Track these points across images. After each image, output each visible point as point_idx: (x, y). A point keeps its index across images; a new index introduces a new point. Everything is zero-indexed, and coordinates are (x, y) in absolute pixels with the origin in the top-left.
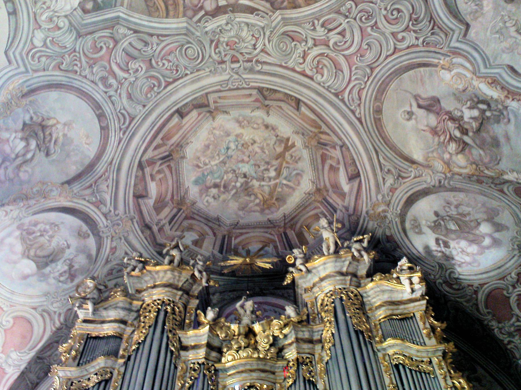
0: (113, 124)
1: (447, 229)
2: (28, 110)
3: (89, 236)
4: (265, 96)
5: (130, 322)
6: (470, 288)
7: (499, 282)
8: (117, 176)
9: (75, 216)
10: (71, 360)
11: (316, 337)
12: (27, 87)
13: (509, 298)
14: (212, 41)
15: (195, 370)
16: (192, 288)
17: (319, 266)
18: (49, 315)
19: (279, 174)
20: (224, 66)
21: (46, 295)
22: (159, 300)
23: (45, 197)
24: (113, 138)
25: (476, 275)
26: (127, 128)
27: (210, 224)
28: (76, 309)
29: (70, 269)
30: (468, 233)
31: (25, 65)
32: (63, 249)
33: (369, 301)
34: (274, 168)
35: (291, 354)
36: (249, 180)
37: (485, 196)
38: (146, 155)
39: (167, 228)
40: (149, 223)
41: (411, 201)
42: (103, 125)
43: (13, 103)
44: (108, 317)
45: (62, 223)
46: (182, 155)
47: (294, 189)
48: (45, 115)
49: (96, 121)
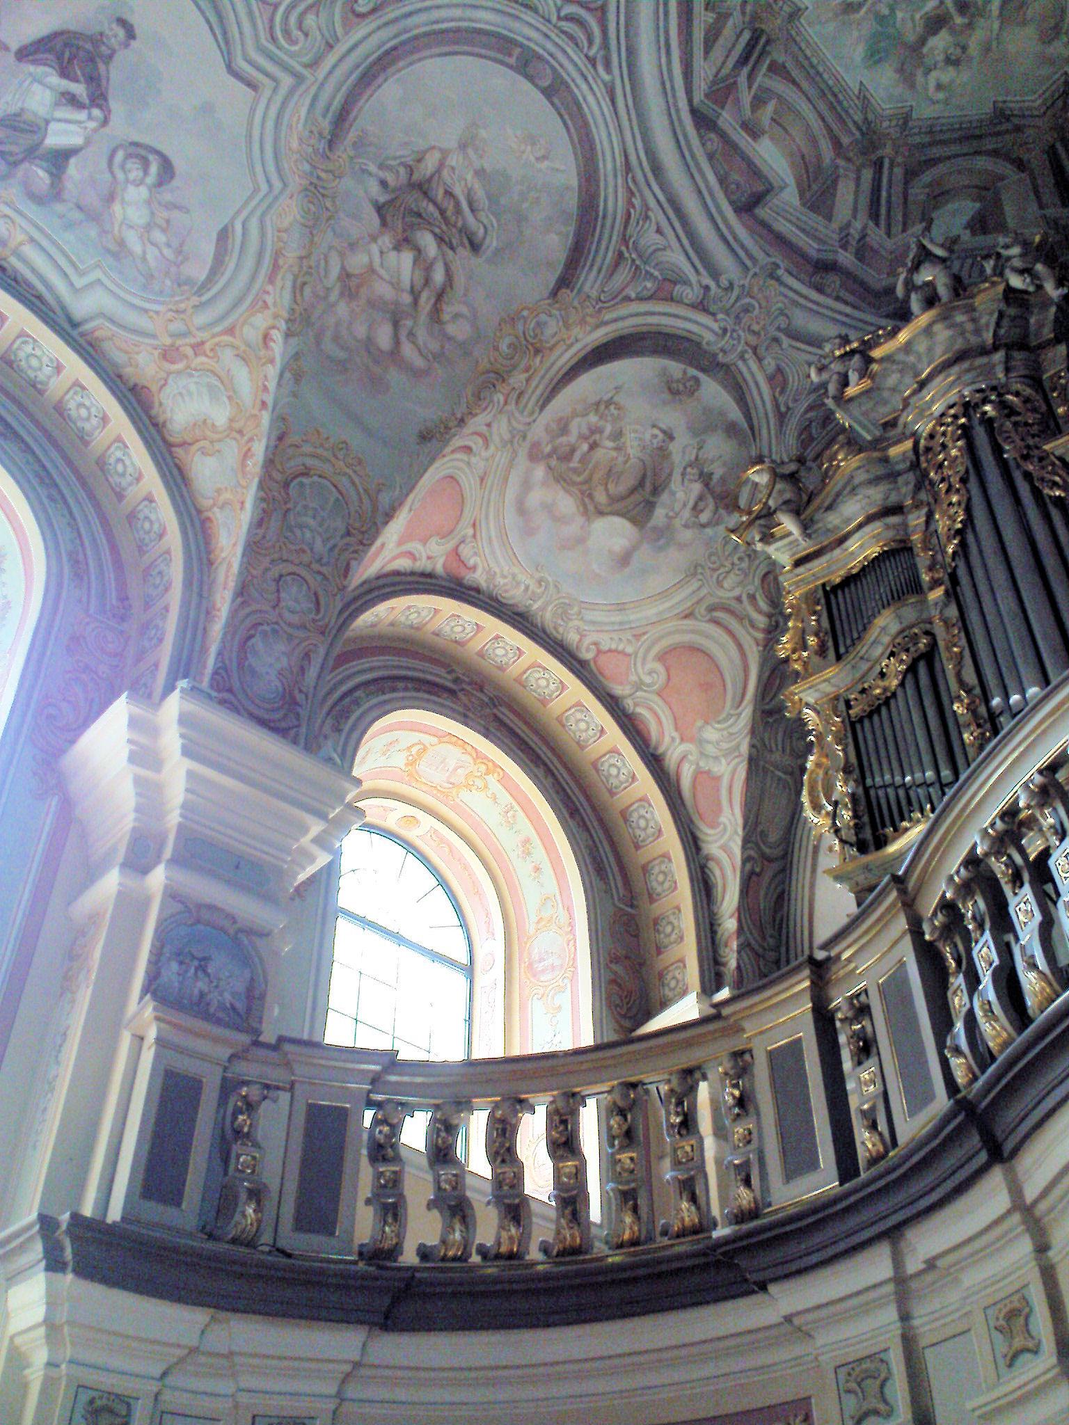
2: (363, 171)
3: (697, 380)
9: (638, 353)
10: (816, 659)
12: (324, 116)
18: (732, 612)
21: (694, 574)
22: (951, 407)
23: (537, 351)
24: (590, 98)
26: (605, 45)
27: (989, 144)
28: (759, 546)
29: (707, 485)
31: (286, 68)
32: (660, 448)
38: (696, 80)
39: (876, 236)
40: (823, 256)
43: (323, 175)
44: (848, 521)
49: (526, 85)
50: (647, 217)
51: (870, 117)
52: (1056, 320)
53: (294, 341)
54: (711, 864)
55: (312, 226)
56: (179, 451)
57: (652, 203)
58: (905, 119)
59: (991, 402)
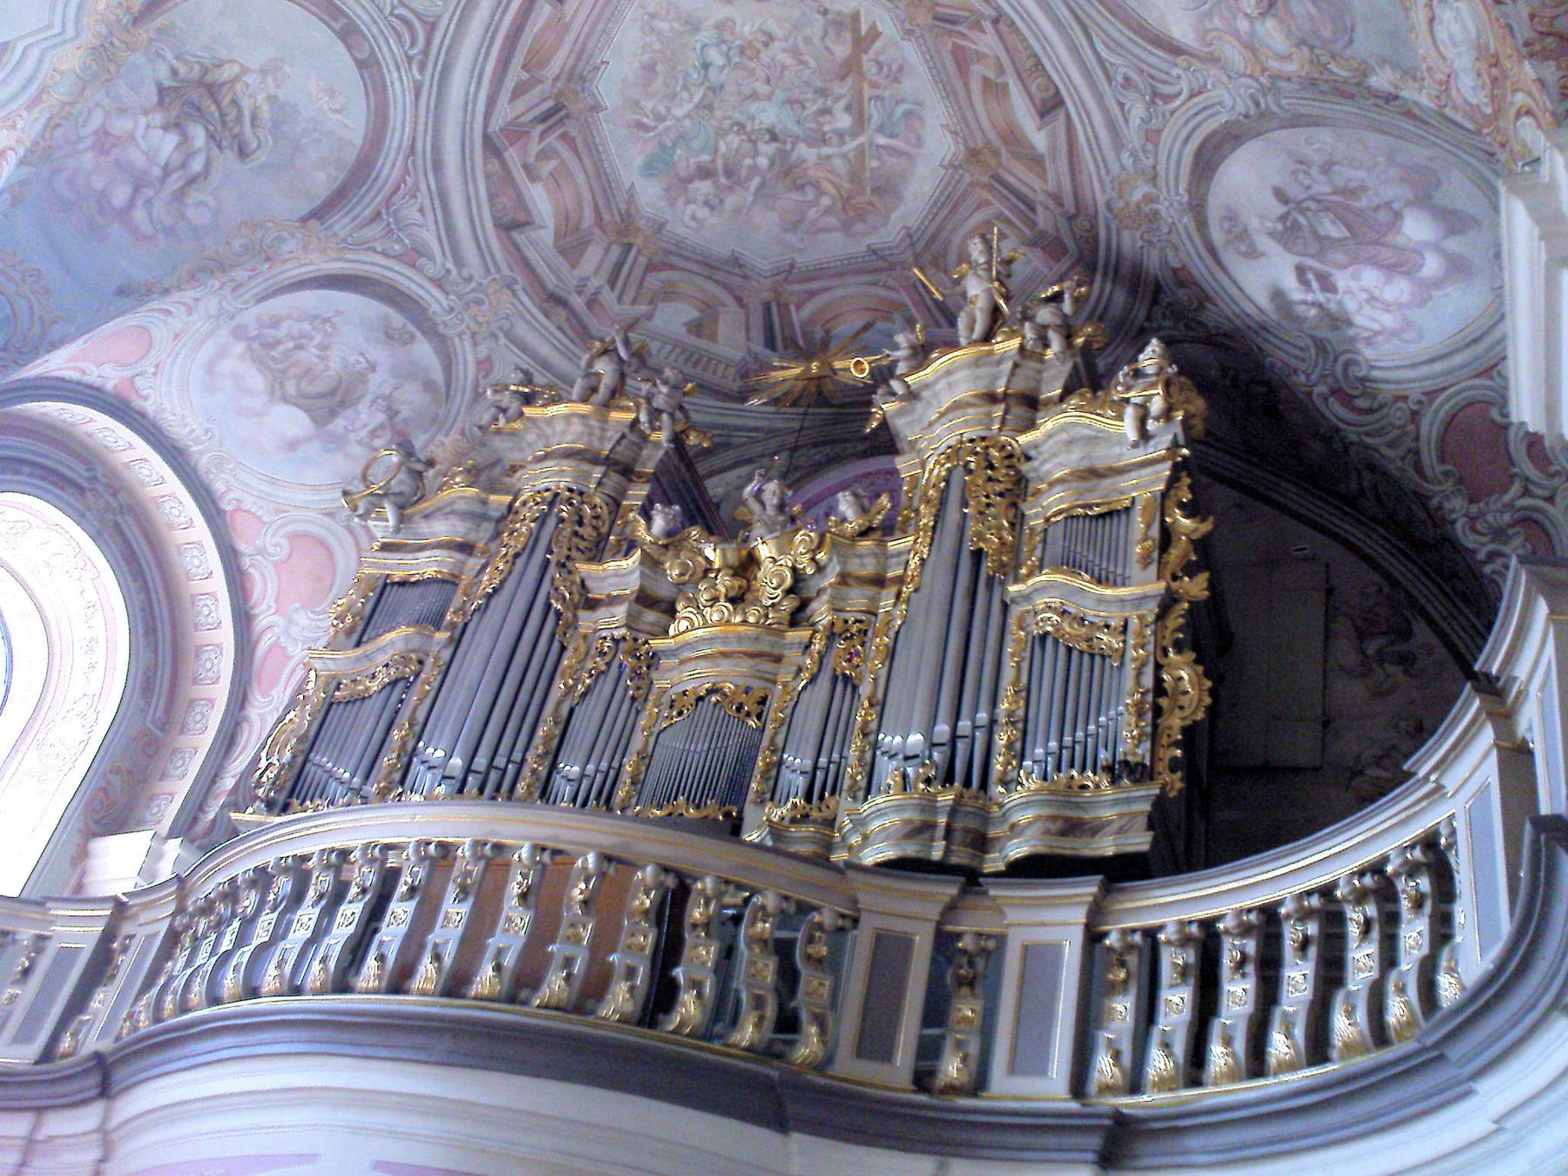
0: (385, 49)
1: (1319, 238)
2: (159, 55)
5: (481, 545)
6: (1400, 404)
7: (1476, 382)
8: (438, 181)
9: (364, 294)
10: (342, 636)
16: (638, 454)
17: (937, 381)
19: (860, 121)
23: (268, 259)
24: (397, 84)
25: (1413, 366)
26: (426, 52)
27: (719, 276)
29: (391, 418)
30: (1376, 243)
33: (1036, 470)
34: (842, 104)
36: (788, 147)
37: (1383, 132)
38: (493, 119)
39: (608, 297)
40: (557, 291)
41: (1206, 163)
42: (361, 56)
43: (116, 42)
45: (338, 313)
46: (590, 101)
49: (340, 48)
50: (414, 196)
51: (633, 211)
52: (661, 460)
53: (26, 170)
54: (245, 726)
55: (84, 83)
57: (423, 186)
59: (571, 504)
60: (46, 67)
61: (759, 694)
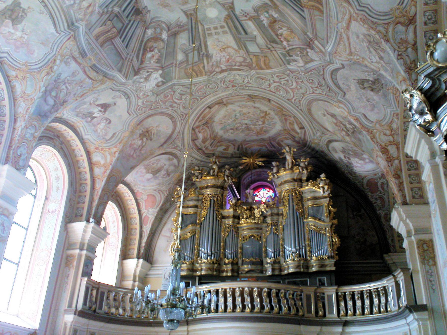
4: (251, 98)
5: (199, 206)
11: (280, 212)
13: (377, 183)
14: (221, 81)
15: (229, 228)
19: (264, 123)
20: (229, 89)
29: (167, 173)
31: (136, 114)
35: (269, 220)
47: (272, 129)
48: (147, 127)
56: (93, 165)
58: (221, 137)
60: (122, 137)
61: (260, 236)
